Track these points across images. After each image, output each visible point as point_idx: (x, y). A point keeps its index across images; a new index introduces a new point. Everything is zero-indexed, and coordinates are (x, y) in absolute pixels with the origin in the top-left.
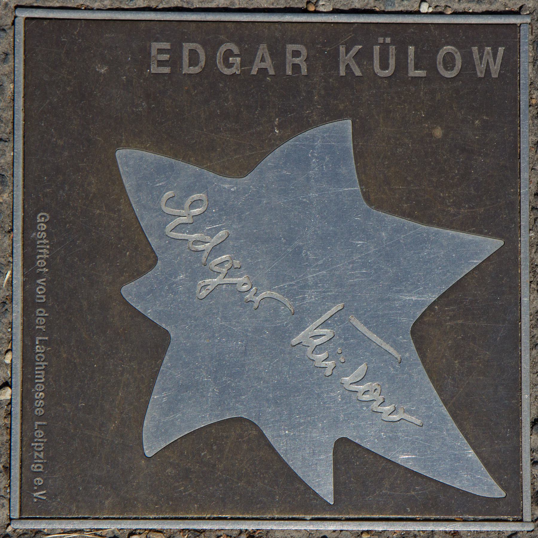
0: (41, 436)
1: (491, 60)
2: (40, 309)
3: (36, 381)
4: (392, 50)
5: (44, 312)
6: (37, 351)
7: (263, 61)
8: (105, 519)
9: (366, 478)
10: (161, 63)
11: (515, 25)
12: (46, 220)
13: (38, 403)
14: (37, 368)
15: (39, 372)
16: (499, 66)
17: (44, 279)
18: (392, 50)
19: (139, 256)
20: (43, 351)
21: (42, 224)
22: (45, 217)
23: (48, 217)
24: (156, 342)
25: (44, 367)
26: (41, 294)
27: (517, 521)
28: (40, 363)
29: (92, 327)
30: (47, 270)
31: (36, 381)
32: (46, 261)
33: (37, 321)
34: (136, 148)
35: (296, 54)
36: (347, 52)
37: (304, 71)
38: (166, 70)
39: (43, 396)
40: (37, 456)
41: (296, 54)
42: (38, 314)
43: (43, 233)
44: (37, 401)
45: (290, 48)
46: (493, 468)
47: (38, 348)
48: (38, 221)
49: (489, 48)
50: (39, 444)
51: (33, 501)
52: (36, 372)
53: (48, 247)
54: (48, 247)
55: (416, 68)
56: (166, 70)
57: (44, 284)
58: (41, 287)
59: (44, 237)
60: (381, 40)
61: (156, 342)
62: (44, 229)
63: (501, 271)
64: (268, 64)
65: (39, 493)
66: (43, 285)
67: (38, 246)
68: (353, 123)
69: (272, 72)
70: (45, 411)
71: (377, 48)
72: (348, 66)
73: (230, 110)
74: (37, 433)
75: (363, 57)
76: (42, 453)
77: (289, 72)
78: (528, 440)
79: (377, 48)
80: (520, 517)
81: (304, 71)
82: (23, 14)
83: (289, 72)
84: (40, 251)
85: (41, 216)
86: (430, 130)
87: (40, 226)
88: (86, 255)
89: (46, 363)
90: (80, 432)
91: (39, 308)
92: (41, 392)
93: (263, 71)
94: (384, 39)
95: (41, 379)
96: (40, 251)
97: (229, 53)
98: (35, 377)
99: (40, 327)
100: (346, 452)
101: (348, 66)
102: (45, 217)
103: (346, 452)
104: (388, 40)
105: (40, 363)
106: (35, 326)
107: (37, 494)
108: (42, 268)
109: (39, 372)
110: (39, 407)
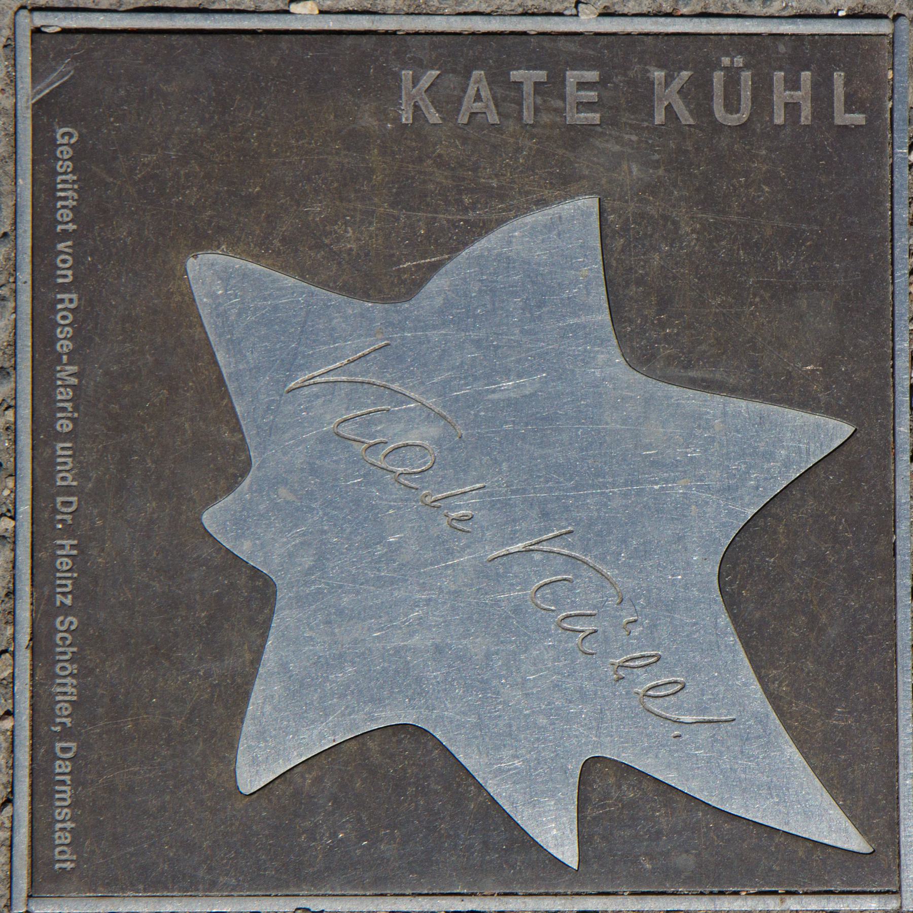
0: (68, 568)
3: (59, 468)
4: (746, 75)
5: (69, 852)
8: (191, 896)
12: (73, 141)
15: (63, 460)
18: (746, 75)
20: (68, 770)
22: (71, 135)
23: (76, 135)
26: (64, 269)
30: (75, 227)
31: (59, 468)
32: (71, 209)
40: (66, 598)
43: (67, 329)
44: (60, 163)
46: (838, 784)
51: (54, 528)
53: (76, 187)
54: (76, 187)
55: (848, 110)
57: (70, 251)
60: (726, 61)
67: (59, 186)
71: (718, 77)
72: (669, 108)
74: (61, 563)
75: (698, 93)
76: (70, 596)
77: (806, 75)
79: (718, 77)
82: (27, 22)
85: (63, 135)
86: (750, 227)
89: (75, 649)
94: (732, 62)
95: (64, 800)
99: (64, 865)
100: (612, 796)
101: (669, 108)
103: (612, 796)
104: (739, 61)
106: (56, 227)
107: (63, 245)
110: (62, 632)
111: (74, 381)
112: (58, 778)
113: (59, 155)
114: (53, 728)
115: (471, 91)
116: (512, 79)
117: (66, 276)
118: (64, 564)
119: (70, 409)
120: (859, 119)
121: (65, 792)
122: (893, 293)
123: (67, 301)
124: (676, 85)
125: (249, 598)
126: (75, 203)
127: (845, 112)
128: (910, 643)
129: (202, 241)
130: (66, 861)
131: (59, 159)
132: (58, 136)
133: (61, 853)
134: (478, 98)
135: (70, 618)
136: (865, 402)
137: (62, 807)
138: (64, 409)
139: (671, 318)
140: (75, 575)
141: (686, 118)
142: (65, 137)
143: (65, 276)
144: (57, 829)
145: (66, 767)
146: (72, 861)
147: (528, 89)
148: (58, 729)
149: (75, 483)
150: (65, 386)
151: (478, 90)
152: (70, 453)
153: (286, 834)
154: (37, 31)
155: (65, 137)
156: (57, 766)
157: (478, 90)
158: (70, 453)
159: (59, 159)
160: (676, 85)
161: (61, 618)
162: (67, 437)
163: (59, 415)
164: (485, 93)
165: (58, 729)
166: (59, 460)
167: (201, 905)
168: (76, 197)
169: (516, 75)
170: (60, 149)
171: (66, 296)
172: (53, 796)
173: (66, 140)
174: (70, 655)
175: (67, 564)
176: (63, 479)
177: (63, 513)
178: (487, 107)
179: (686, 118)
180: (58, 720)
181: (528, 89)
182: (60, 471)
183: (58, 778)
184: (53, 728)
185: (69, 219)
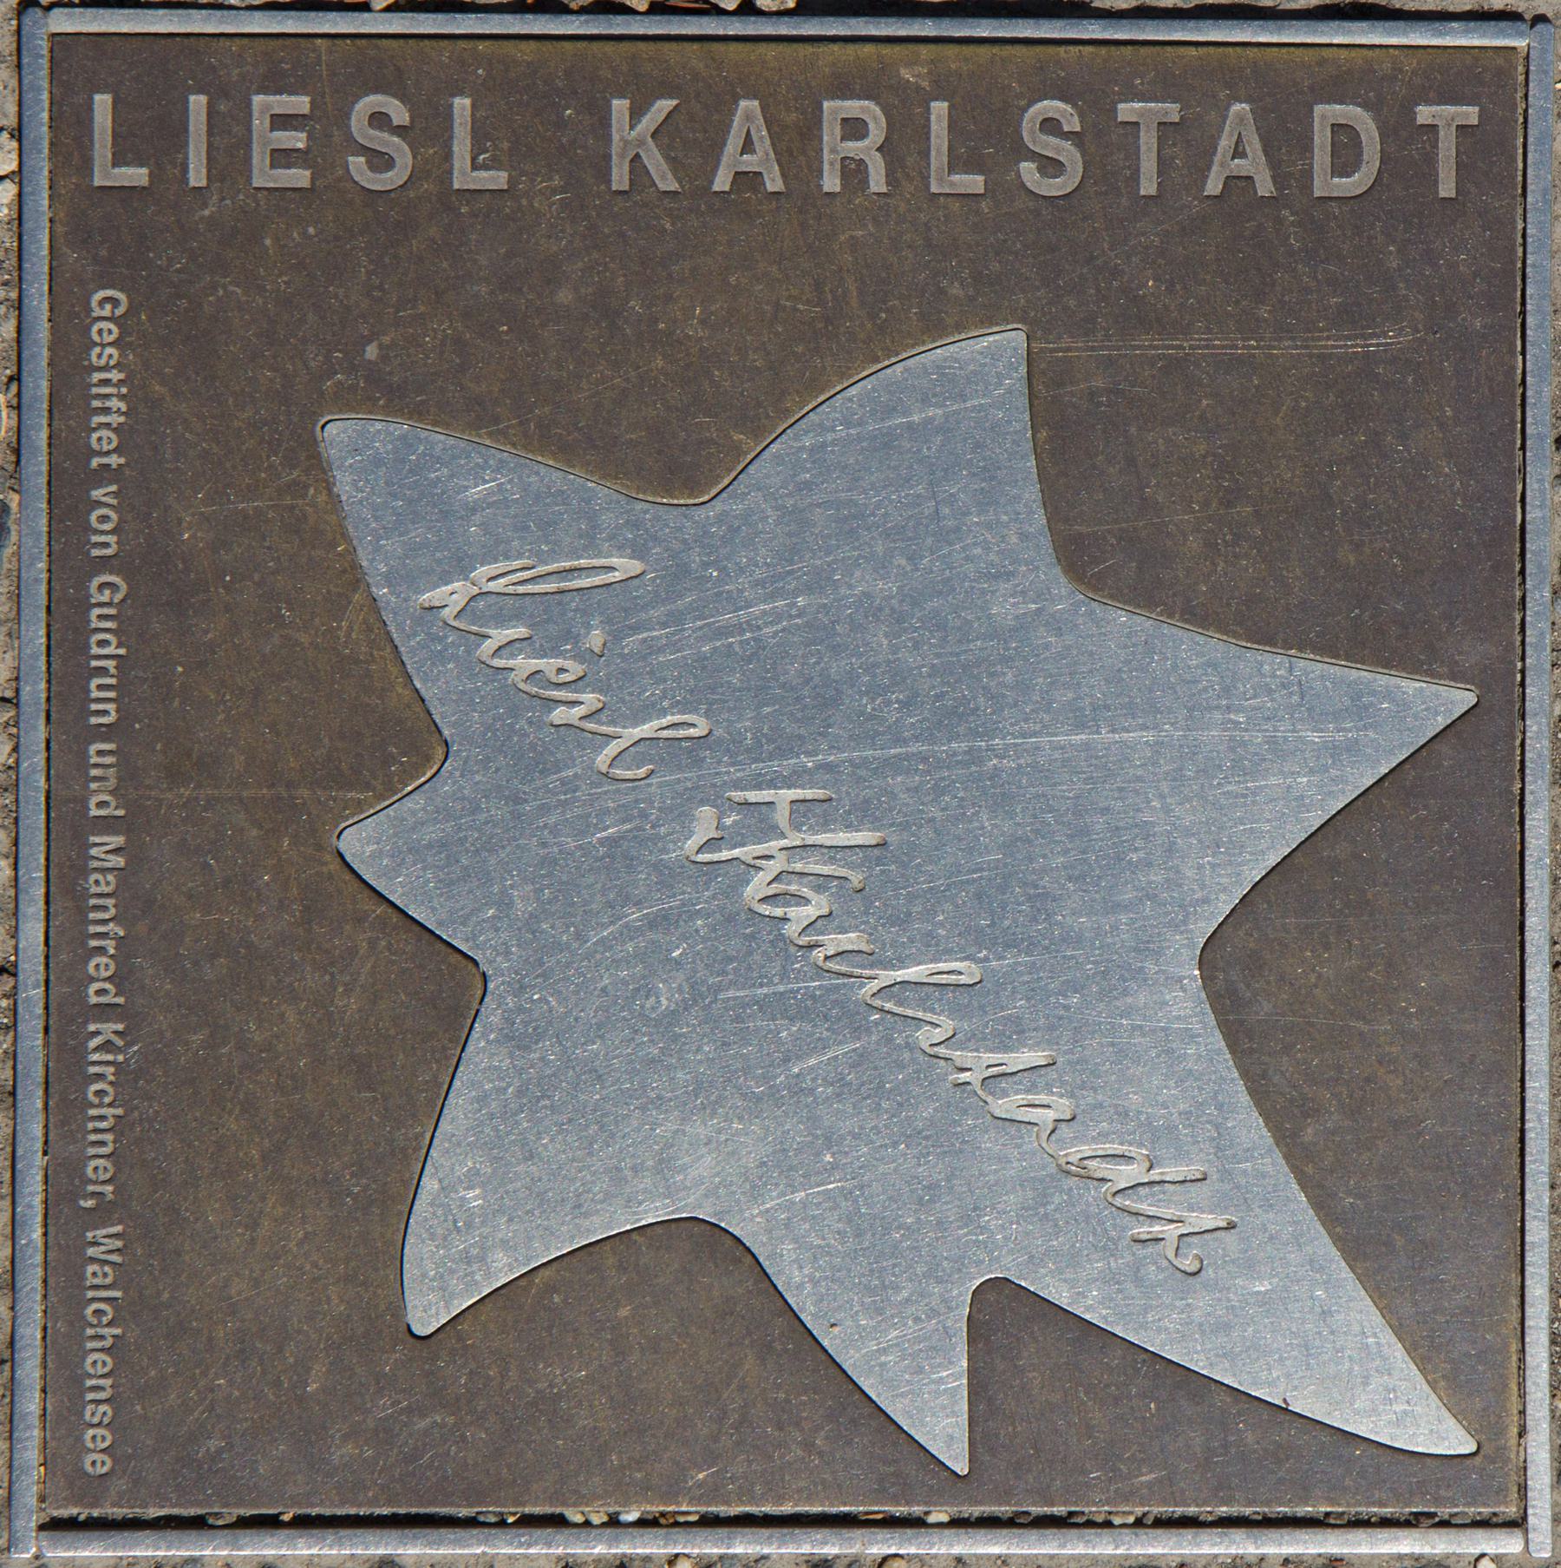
2: (109, 293)
5: (113, 804)
6: (94, 889)
10: (282, 157)
12: (120, 311)
14: (90, 1126)
17: (114, 488)
19: (390, 742)
24: (443, 989)
25: (108, 1343)
26: (103, 532)
28: (103, 1111)
29: (274, 1000)
30: (122, 461)
32: (115, 430)
33: (89, 1171)
35: (854, 128)
36: (636, 113)
37: (877, 182)
38: (299, 177)
41: (854, 128)
42: (97, 312)
43: (109, 350)
44: (98, 350)
45: (834, 109)
47: (94, 1274)
48: (93, 601)
49: (748, 105)
54: (124, 390)
56: (299, 177)
57: (114, 502)
58: (107, 527)
61: (443, 989)
63: (1483, 745)
64: (1256, 167)
65: (104, 1232)
68: (1122, 101)
69: (774, 183)
70: (115, 1461)
74: (94, 1463)
77: (831, 182)
80: (1511, 1511)
81: (877, 182)
83: (831, 182)
85: (102, 587)
87: (94, 1463)
88: (246, 715)
92: (109, 344)
98: (87, 774)
99: (105, 460)
100: (1005, 1320)
102: (115, 302)
103: (1005, 1320)
105: (103, 1111)
106: (89, 461)
108: (108, 453)
109: (99, 1137)
111: (119, 861)
113: (95, 445)
114: (82, 1203)
115: (733, 143)
117: (105, 543)
119: (113, 671)
120: (137, 175)
122: (1523, 745)
124: (650, 121)
126: (122, 419)
127: (272, 166)
128: (1554, 434)
130: (107, 396)
131: (96, 344)
132: (94, 304)
137: (98, 1402)
138: (103, 671)
140: (118, 1294)
141: (93, 1043)
142: (106, 306)
144: (95, 380)
145: (108, 883)
147: (1148, 142)
148: (90, 1203)
149: (121, 812)
150: (103, 871)
152: (112, 695)
154: (1518, 1523)
156: (89, 1275)
159: (96, 344)
160: (650, 121)
162: (107, 732)
163: (90, 1345)
164: (1254, 145)
165: (90, 1203)
168: (124, 409)
169: (1127, 110)
172: (82, 1383)
173: (107, 311)
174: (112, 1120)
175: (104, 1363)
176: (101, 805)
177: (103, 532)
179: (93, 1043)
180: (91, 1188)
181: (1148, 142)
184: (82, 1203)
185: (111, 447)
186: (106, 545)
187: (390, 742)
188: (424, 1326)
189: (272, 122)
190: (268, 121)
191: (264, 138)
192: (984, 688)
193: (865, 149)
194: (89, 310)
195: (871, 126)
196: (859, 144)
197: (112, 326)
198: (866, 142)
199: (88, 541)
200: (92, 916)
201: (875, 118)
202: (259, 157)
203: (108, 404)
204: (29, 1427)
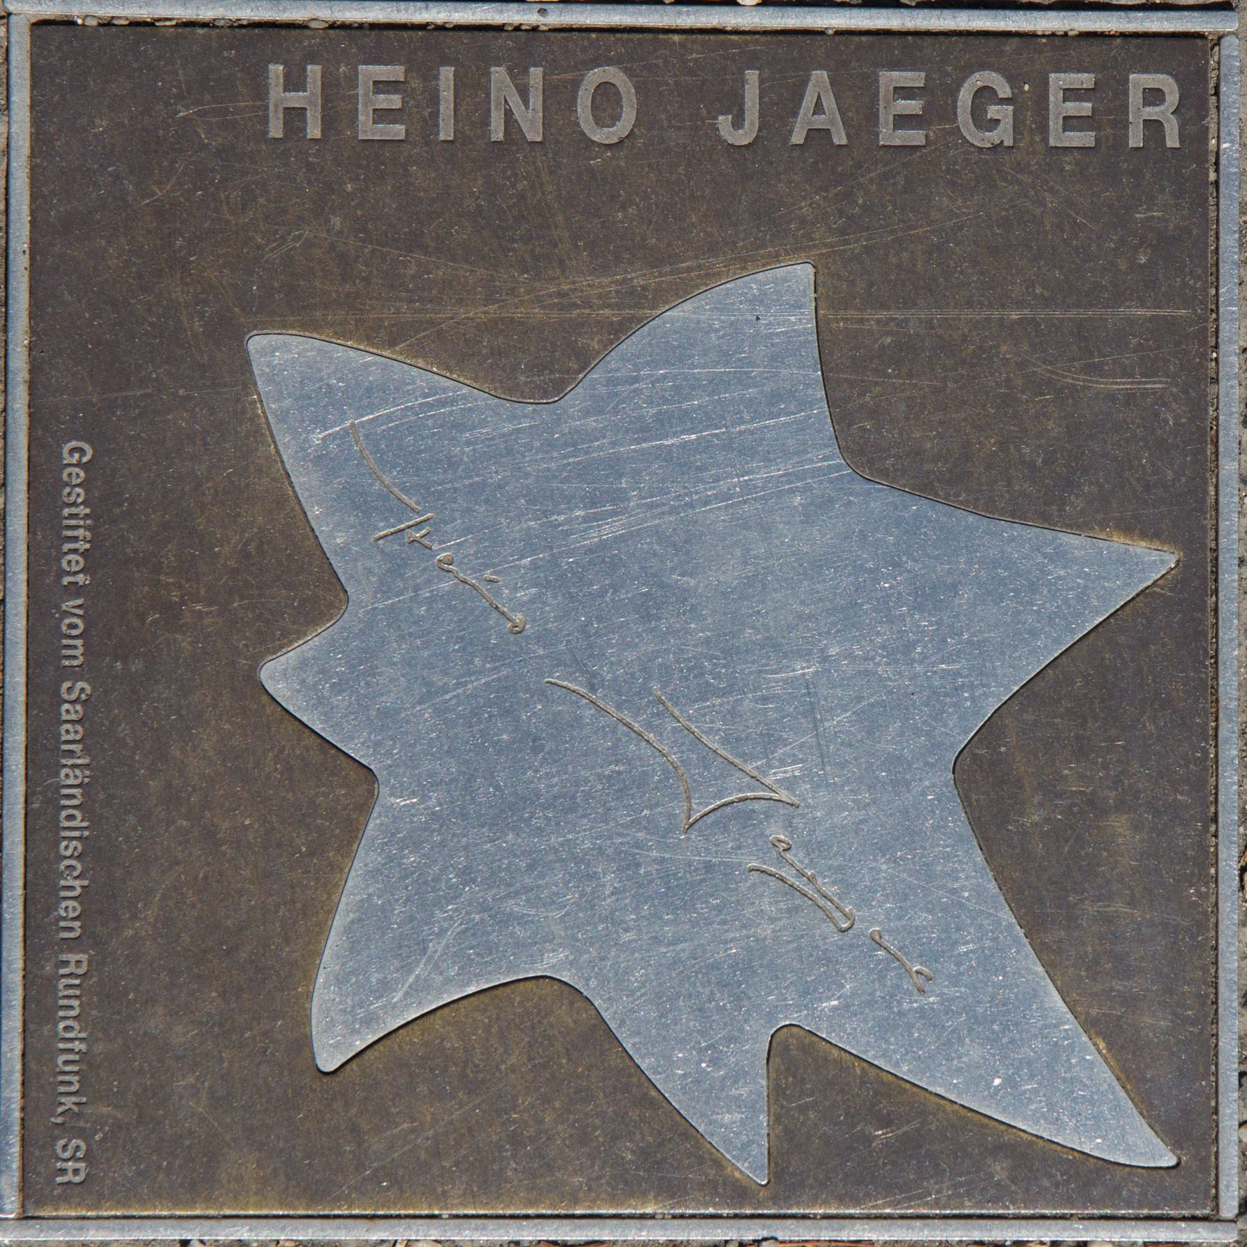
0: (75, 915)
1: (515, 101)
2: (74, 444)
5: (79, 818)
6: (65, 717)
7: (819, 105)
9: (853, 1126)
11: (1200, 36)
12: (85, 460)
13: (67, 847)
16: (540, 108)
17: (79, 602)
21: (77, 470)
22: (82, 452)
27: (1205, 1219)
32: (82, 554)
34: (342, 333)
35: (1154, 96)
37: (314, 130)
39: (80, 849)
41: (1154, 96)
44: (67, 490)
45: (1139, 81)
50: (73, 823)
52: (61, 1046)
53: (89, 522)
54: (89, 522)
57: (80, 612)
58: (75, 632)
59: (80, 500)
62: (79, 481)
66: (79, 616)
73: (513, 233)
74: (70, 475)
75: (559, 98)
77: (276, 130)
78: (1232, 1026)
81: (314, 130)
83: (276, 130)
84: (69, 533)
85: (72, 451)
87: (69, 562)
88: (178, 576)
90: (175, 1023)
91: (69, 441)
93: (818, 136)
95: (75, 657)
96: (69, 533)
97: (985, 95)
98: (56, 1003)
99: (71, 579)
100: (799, 1064)
102: (82, 452)
103: (799, 1064)
107: (71, 603)
108: (76, 573)
112: (65, 747)
115: (808, 102)
116: (1177, 145)
118: (73, 563)
121: (75, 647)
123: (73, 964)
125: (325, 793)
126: (88, 546)
129: (296, 309)
130: (77, 527)
131: (67, 484)
133: (67, 1028)
134: (818, 108)
135: (80, 685)
136: (1184, 515)
138: (71, 753)
139: (922, 419)
142: (74, 455)
143: (71, 929)
145: (76, 732)
146: (81, 1040)
151: (819, 97)
153: (326, 1136)
155: (74, 455)
156: (63, 732)
157: (819, 97)
158: (76, 1068)
159: (67, 484)
161: (62, 1142)
164: (829, 102)
166: (61, 1002)
167: (406, 10)
170: (68, 470)
171: (72, 958)
175: (77, 562)
178: (832, 122)
182: (65, 807)
183: (65, 747)
186: (71, 929)
187: (299, 587)
188: (329, 1067)
189: (1064, 124)
190: (1061, 121)
191: (1059, 108)
192: (453, 426)
193: (1163, 112)
194: (61, 457)
195: (1166, 90)
196: (1157, 109)
197: (75, 904)
198: (1162, 108)
199: (58, 762)
200: (63, 894)
201: (968, 130)
202: (1055, 124)
203: (75, 533)
204: (12, 1091)
